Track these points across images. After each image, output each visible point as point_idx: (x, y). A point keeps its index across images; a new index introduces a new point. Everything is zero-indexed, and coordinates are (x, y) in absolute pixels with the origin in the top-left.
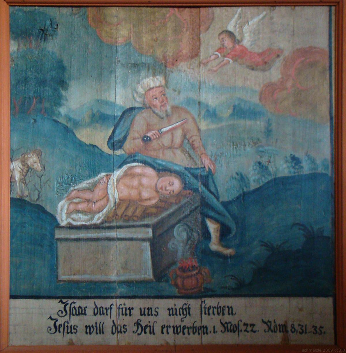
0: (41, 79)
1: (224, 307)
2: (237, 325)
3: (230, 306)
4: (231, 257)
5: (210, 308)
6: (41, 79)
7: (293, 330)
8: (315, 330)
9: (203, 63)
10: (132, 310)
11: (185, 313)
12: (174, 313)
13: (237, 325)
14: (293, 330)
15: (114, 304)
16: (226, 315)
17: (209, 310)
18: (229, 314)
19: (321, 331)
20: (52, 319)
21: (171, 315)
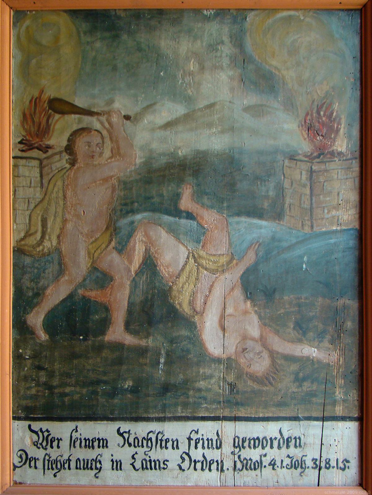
0: (243, 105)
1: (265, 438)
2: (259, 461)
3: (174, 439)
4: (344, 381)
5: (199, 440)
6: (243, 105)
7: (328, 466)
8: (315, 463)
9: (104, 265)
10: (60, 441)
11: (150, 444)
12: (252, 442)
13: (259, 461)
14: (328, 466)
15: (29, 424)
16: (292, 447)
17: (166, 442)
18: (173, 448)
19: (345, 465)
20: (290, 458)
21: (298, 447)
